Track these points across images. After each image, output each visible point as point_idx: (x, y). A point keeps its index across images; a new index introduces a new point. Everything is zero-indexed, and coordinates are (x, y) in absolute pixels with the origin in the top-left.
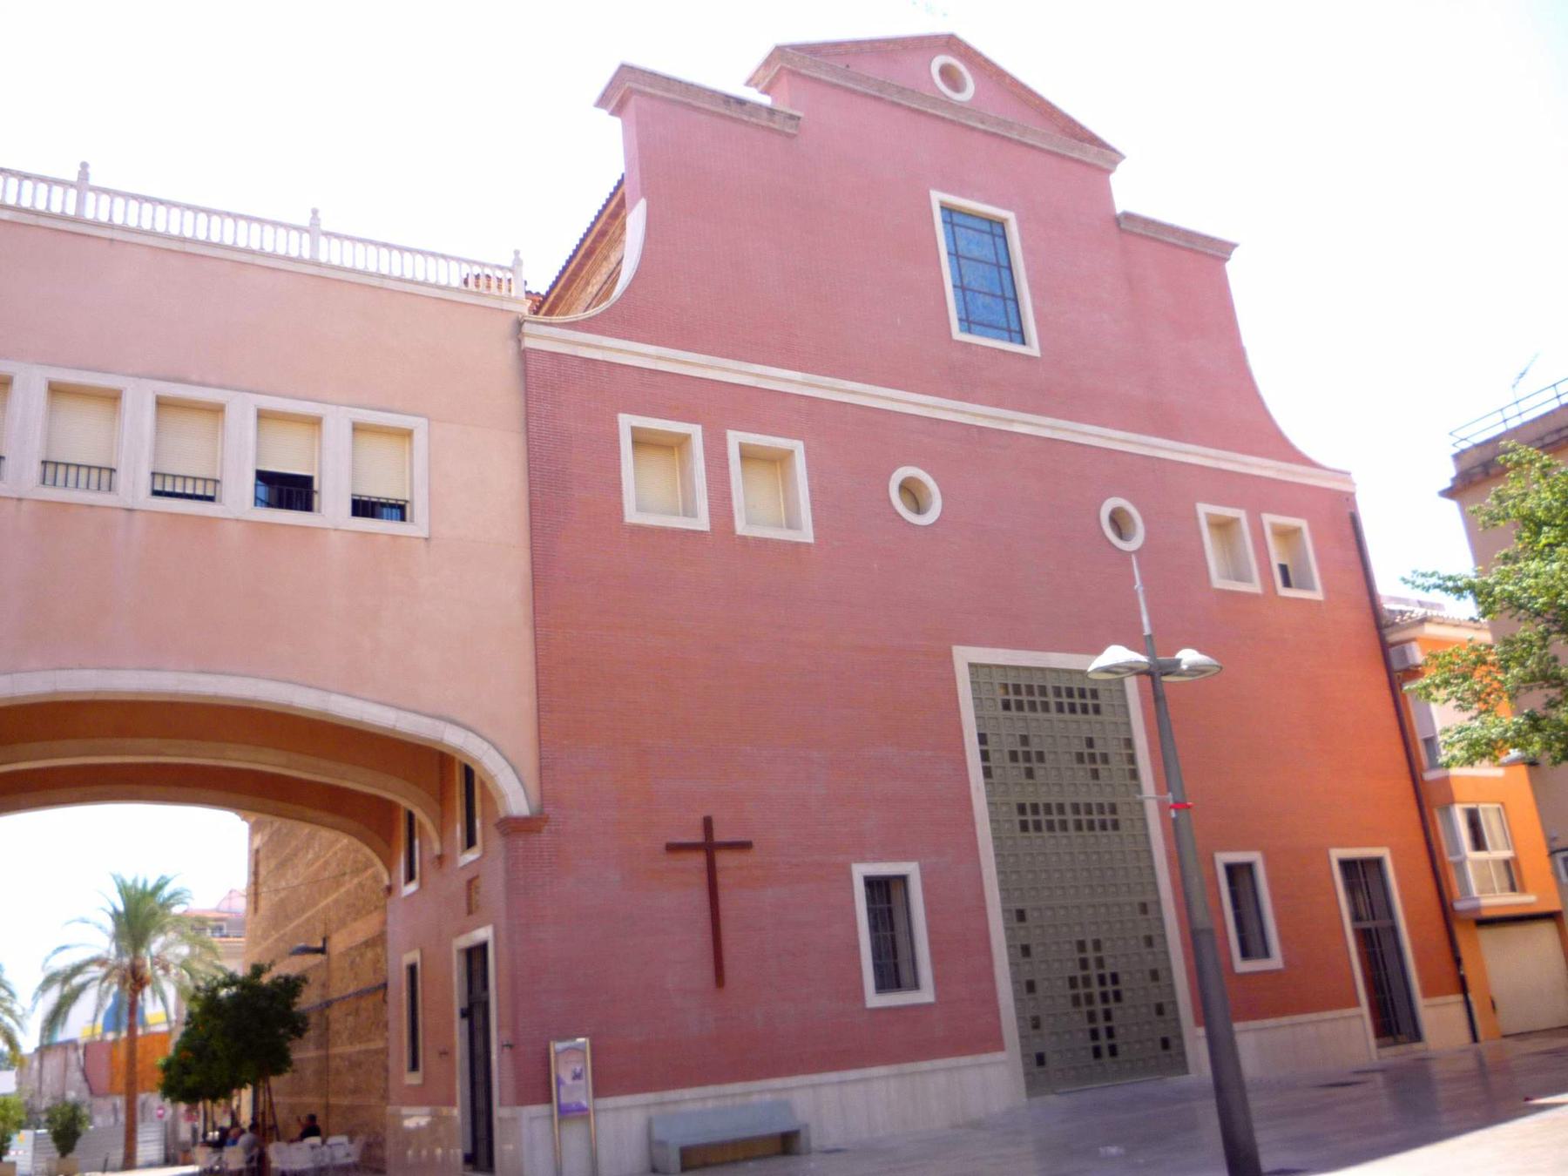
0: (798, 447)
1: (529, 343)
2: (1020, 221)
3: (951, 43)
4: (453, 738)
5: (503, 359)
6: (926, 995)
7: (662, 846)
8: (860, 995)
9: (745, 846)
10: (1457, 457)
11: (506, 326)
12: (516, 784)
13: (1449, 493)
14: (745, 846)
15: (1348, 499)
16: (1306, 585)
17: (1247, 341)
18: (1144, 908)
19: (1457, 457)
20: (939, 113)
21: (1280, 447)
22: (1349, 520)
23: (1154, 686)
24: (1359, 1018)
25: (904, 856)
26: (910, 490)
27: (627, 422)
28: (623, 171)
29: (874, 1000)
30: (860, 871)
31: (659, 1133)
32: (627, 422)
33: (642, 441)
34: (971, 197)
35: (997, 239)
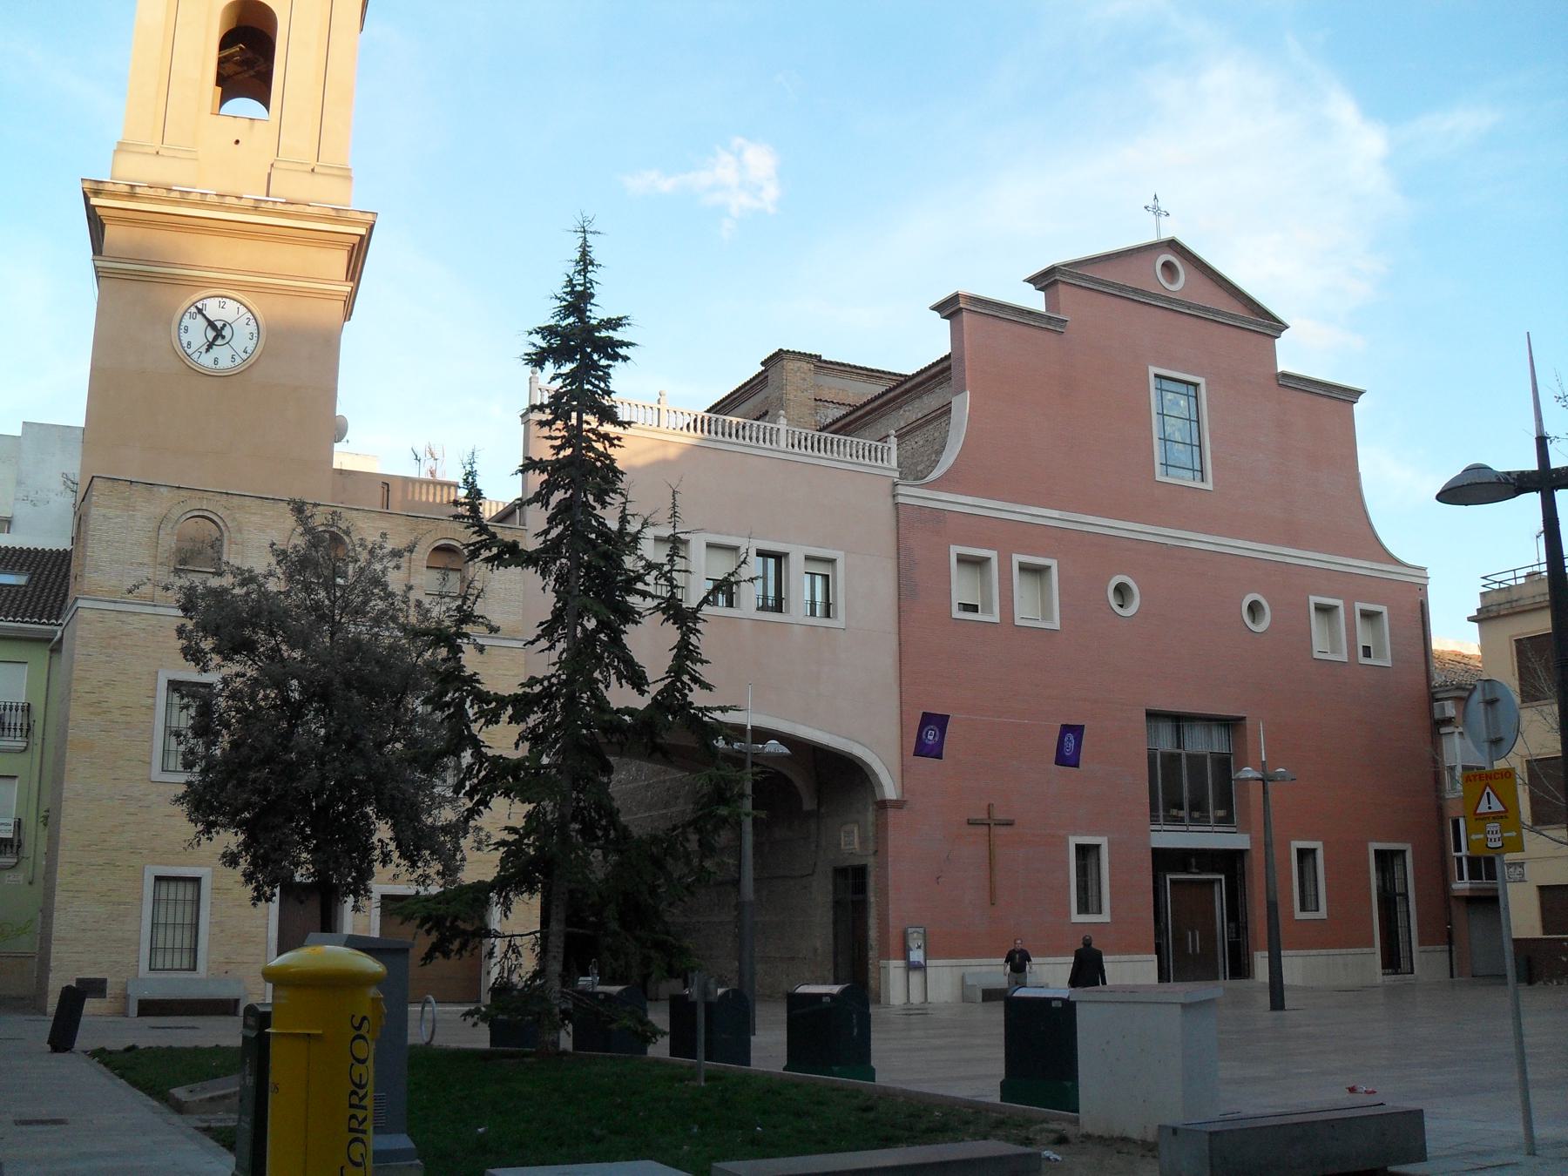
0: (1053, 563)
1: (901, 499)
2: (1207, 384)
3: (1173, 245)
4: (857, 750)
5: (887, 506)
6: (1105, 917)
7: (965, 820)
8: (1068, 913)
9: (1010, 824)
10: (1483, 595)
11: (887, 484)
12: (890, 780)
13: (1471, 619)
14: (1010, 824)
15: (1422, 589)
16: (1380, 656)
17: (1361, 469)
18: (1022, 597)
19: (1483, 595)
20: (1159, 304)
21: (1375, 548)
22: (1419, 605)
23: (1264, 787)
24: (1374, 956)
25: (1100, 834)
26: (1121, 590)
27: (955, 550)
28: (950, 351)
29: (1077, 918)
30: (1074, 840)
31: (969, 982)
32: (955, 550)
33: (962, 560)
34: (1175, 369)
35: (1194, 448)
